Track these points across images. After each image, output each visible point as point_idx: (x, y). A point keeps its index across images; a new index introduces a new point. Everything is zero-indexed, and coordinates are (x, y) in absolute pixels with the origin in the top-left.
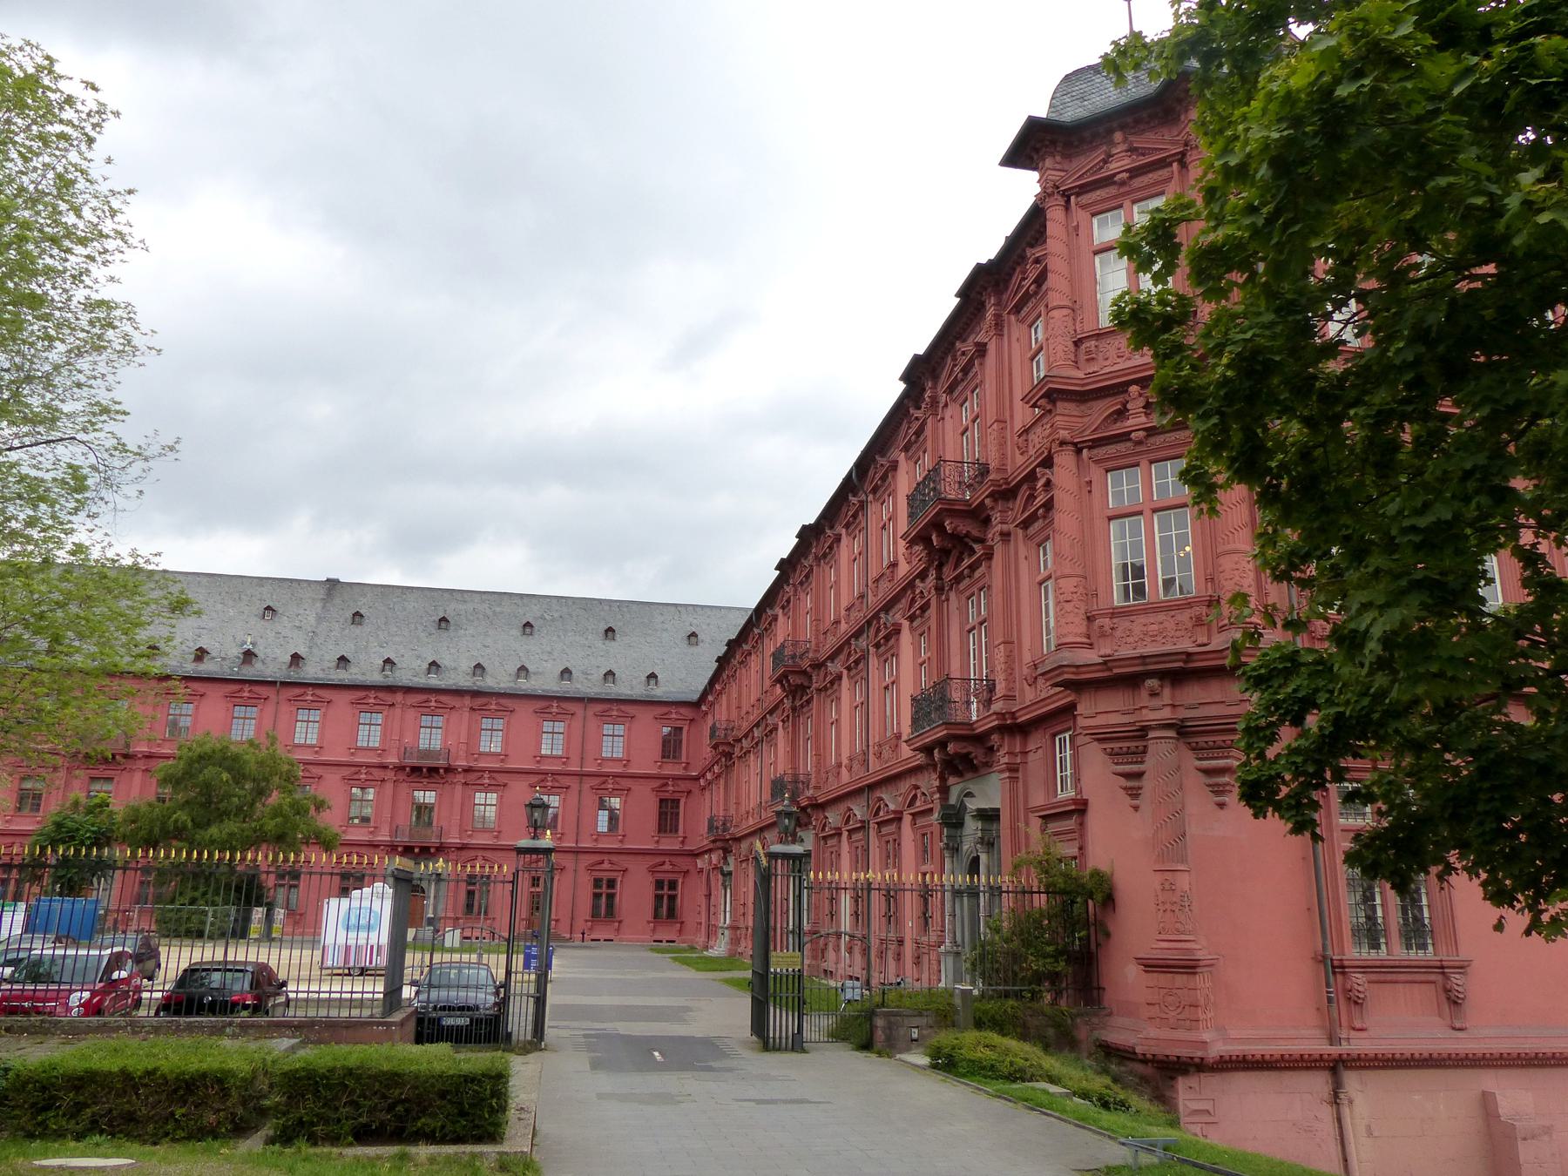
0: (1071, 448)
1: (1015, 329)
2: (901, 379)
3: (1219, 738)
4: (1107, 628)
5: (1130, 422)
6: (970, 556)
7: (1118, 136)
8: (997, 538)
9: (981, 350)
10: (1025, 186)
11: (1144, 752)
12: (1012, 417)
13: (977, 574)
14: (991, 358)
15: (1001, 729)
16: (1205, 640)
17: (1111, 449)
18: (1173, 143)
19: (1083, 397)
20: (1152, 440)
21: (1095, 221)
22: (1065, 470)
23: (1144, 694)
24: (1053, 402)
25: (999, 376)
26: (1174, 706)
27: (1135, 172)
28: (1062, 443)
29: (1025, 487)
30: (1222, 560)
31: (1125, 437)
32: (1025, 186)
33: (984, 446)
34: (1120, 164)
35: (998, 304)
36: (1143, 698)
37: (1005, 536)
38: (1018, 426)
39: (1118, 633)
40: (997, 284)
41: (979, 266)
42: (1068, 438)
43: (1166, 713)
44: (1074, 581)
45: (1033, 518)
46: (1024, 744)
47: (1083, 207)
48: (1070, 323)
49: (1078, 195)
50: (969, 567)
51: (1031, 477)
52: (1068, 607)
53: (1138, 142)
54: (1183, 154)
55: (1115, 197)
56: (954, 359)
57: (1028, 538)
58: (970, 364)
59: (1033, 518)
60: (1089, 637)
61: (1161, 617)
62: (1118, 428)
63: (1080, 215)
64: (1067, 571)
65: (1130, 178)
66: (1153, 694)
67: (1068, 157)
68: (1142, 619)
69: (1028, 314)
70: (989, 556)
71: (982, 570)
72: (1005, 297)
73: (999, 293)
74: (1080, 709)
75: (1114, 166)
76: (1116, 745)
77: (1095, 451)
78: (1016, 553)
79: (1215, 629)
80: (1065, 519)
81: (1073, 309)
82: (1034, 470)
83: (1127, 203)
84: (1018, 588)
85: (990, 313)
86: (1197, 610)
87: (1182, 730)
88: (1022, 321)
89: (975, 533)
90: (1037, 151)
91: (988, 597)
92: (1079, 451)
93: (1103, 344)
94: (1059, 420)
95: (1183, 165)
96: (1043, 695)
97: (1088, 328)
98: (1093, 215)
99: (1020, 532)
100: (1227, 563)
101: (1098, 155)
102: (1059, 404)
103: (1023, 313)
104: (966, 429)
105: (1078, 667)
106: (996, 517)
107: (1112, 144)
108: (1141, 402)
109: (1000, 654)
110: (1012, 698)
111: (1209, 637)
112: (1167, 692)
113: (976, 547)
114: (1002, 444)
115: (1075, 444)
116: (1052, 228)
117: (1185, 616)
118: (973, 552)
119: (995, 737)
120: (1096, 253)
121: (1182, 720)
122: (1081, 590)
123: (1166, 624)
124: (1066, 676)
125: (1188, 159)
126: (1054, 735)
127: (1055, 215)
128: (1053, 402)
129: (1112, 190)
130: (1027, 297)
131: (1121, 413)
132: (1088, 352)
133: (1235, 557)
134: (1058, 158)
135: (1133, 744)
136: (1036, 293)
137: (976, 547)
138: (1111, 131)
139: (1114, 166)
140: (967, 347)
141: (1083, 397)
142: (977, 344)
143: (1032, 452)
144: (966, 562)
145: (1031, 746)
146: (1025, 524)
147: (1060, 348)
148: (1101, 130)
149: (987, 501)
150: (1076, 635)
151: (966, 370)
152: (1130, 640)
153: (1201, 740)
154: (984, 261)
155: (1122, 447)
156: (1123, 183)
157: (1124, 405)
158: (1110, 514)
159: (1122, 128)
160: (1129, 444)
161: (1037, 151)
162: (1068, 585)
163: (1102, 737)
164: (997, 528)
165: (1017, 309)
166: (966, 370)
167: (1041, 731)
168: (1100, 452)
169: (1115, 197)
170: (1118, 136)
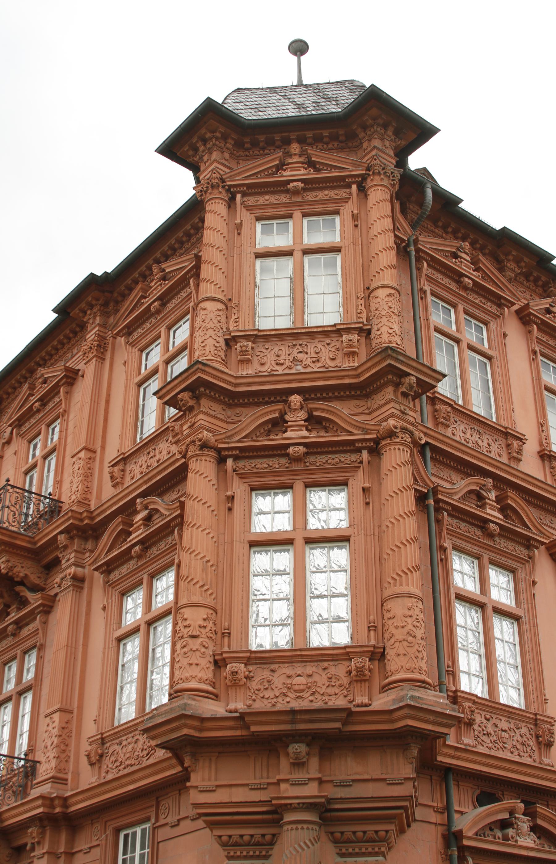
0: (213, 453)
1: (123, 352)
2: (55, 310)
3: (371, 828)
4: (241, 675)
5: (289, 434)
6: (19, 609)
7: (295, 148)
8: (68, 582)
9: (72, 377)
10: (178, 185)
11: (272, 843)
12: (103, 447)
13: (25, 632)
14: (83, 391)
15: (39, 820)
16: (365, 700)
17: (262, 464)
18: (356, 165)
19: (234, 399)
20: (312, 459)
21: (259, 226)
22: (202, 480)
23: (284, 763)
24: (197, 398)
25: (95, 402)
26: (321, 781)
27: (310, 185)
28: (205, 446)
29: (119, 519)
30: (389, 605)
31: (281, 450)
32: (178, 185)
33: (58, 483)
34: (297, 172)
35: (103, 326)
36: (284, 770)
37: (78, 581)
38: (111, 454)
39: (254, 685)
40: (106, 305)
41: (92, 277)
42: (213, 440)
43: (311, 790)
44: (203, 613)
45: (125, 557)
46: (71, 841)
47: (248, 208)
48: (223, 320)
49: (244, 195)
50: (16, 622)
51: (128, 509)
52: (195, 644)
53: (317, 155)
54: (364, 178)
55: (286, 205)
56: (32, 387)
57: (109, 584)
58: (54, 391)
59: (125, 557)
60: (213, 685)
61: (310, 669)
62: (273, 440)
63: (244, 216)
64: (196, 599)
65: (305, 190)
66: (298, 764)
67: (237, 158)
68: (286, 669)
69: (143, 336)
70: (48, 608)
71: (37, 624)
72: (111, 320)
73: (106, 315)
74: (195, 779)
75: (287, 174)
76: (235, 832)
77: (241, 463)
78: (89, 604)
79: (376, 688)
80: (197, 538)
81: (228, 306)
82: (134, 500)
83: (297, 215)
84: (86, 645)
85: (91, 335)
86: (356, 662)
87: (327, 814)
88: (133, 345)
89: (34, 579)
90: (205, 141)
91: (40, 658)
92: (221, 461)
93: (260, 348)
94: (202, 419)
95: (363, 190)
96: (110, 777)
97: (244, 326)
98: (258, 219)
99: (99, 578)
100: (397, 608)
101: (272, 160)
102: (204, 402)
103: (135, 335)
104: (34, 466)
105: (203, 720)
106: (68, 559)
107: (289, 155)
108: (302, 415)
109: (51, 727)
110: (64, 781)
111: (370, 699)
112: (314, 763)
113: (30, 596)
114: (88, 476)
115: (219, 451)
116: (210, 220)
117: (340, 670)
118: (24, 602)
119: (33, 831)
120: (259, 256)
121: (330, 801)
122: (210, 625)
123: (316, 678)
124: (185, 731)
125: (369, 183)
126: (117, 831)
127: (216, 216)
128: (197, 398)
129: (283, 198)
130: (147, 314)
131: (278, 424)
132: (244, 352)
133: (409, 602)
134: (227, 155)
135: (257, 831)
136: (158, 312)
137: (30, 596)
138: (287, 142)
139: (287, 174)
140: (53, 372)
141: (234, 399)
142: (67, 369)
143: (128, 482)
144: (14, 616)
145: (82, 844)
146: (108, 568)
147: (210, 342)
148: (277, 137)
149: (61, 538)
150: (200, 681)
151: (44, 401)
152: (267, 694)
153: (348, 829)
154: (99, 273)
155: (276, 463)
156: (296, 192)
157: (283, 414)
158: (252, 539)
159: (301, 141)
160: (283, 460)
161: (205, 141)
162: (195, 617)
163: (215, 819)
164: (68, 569)
165: (129, 330)
166: (44, 401)
167: (98, 826)
168: (248, 465)
169: (286, 205)
170: (295, 148)
